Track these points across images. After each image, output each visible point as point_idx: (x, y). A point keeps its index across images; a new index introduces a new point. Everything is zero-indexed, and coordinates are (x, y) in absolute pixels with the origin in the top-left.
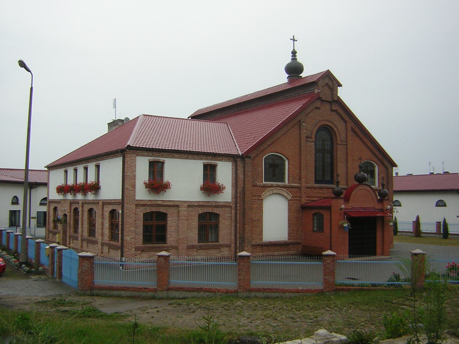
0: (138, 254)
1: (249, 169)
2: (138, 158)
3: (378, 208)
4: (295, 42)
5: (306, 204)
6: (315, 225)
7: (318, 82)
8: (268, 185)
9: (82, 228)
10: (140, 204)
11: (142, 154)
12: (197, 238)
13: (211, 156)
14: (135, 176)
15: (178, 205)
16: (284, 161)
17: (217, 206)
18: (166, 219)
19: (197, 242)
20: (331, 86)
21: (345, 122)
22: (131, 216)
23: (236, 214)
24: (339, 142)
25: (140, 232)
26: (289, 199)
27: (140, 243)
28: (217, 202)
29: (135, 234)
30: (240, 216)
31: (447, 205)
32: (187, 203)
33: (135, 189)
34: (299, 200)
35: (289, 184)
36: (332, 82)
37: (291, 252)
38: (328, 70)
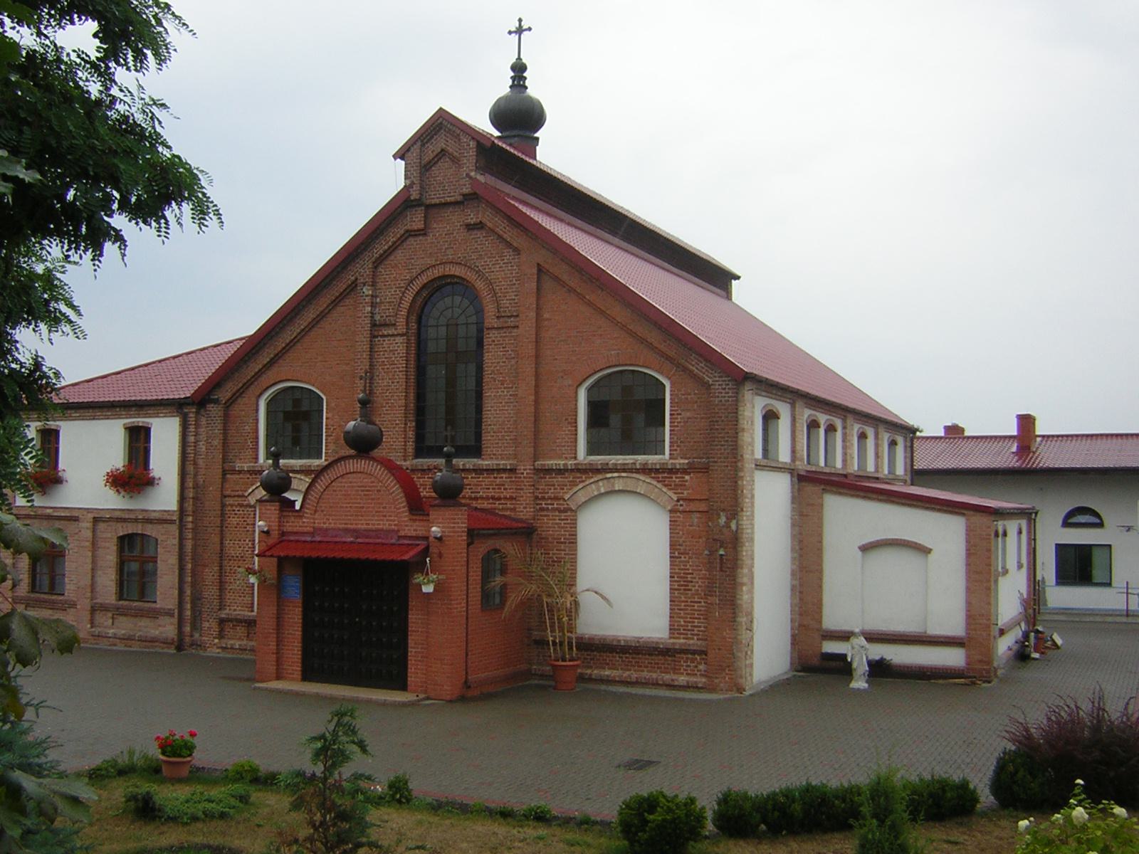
8: (422, 465)
13: (134, 409)
17: (149, 521)
23: (182, 539)
28: (146, 511)
38: (441, 109)
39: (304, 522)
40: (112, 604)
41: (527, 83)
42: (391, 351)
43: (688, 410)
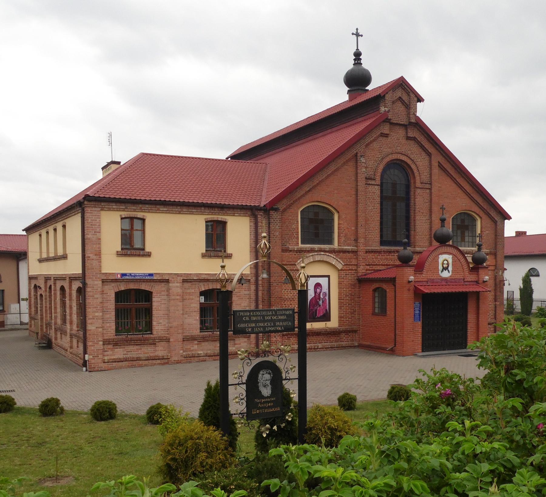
0: (109, 349)
1: (277, 227)
2: (103, 213)
3: (470, 280)
4: (360, 38)
5: (365, 275)
6: (377, 305)
7: (384, 96)
9: (56, 313)
10: (107, 280)
11: (110, 207)
12: (199, 326)
14: (100, 239)
15: (168, 280)
16: (333, 214)
18: (152, 300)
19: (199, 331)
20: (406, 101)
21: (428, 155)
22: (96, 296)
23: (257, 290)
24: (418, 184)
25: (111, 318)
26: (340, 269)
27: (112, 333)
29: (103, 321)
30: (262, 294)
31: (540, 275)
32: (182, 276)
33: (100, 257)
34: (356, 270)
35: (340, 247)
36: (409, 95)
37: (342, 343)
39: (423, 276)
40: (198, 335)
41: (362, 62)
42: (373, 192)
43: (488, 230)
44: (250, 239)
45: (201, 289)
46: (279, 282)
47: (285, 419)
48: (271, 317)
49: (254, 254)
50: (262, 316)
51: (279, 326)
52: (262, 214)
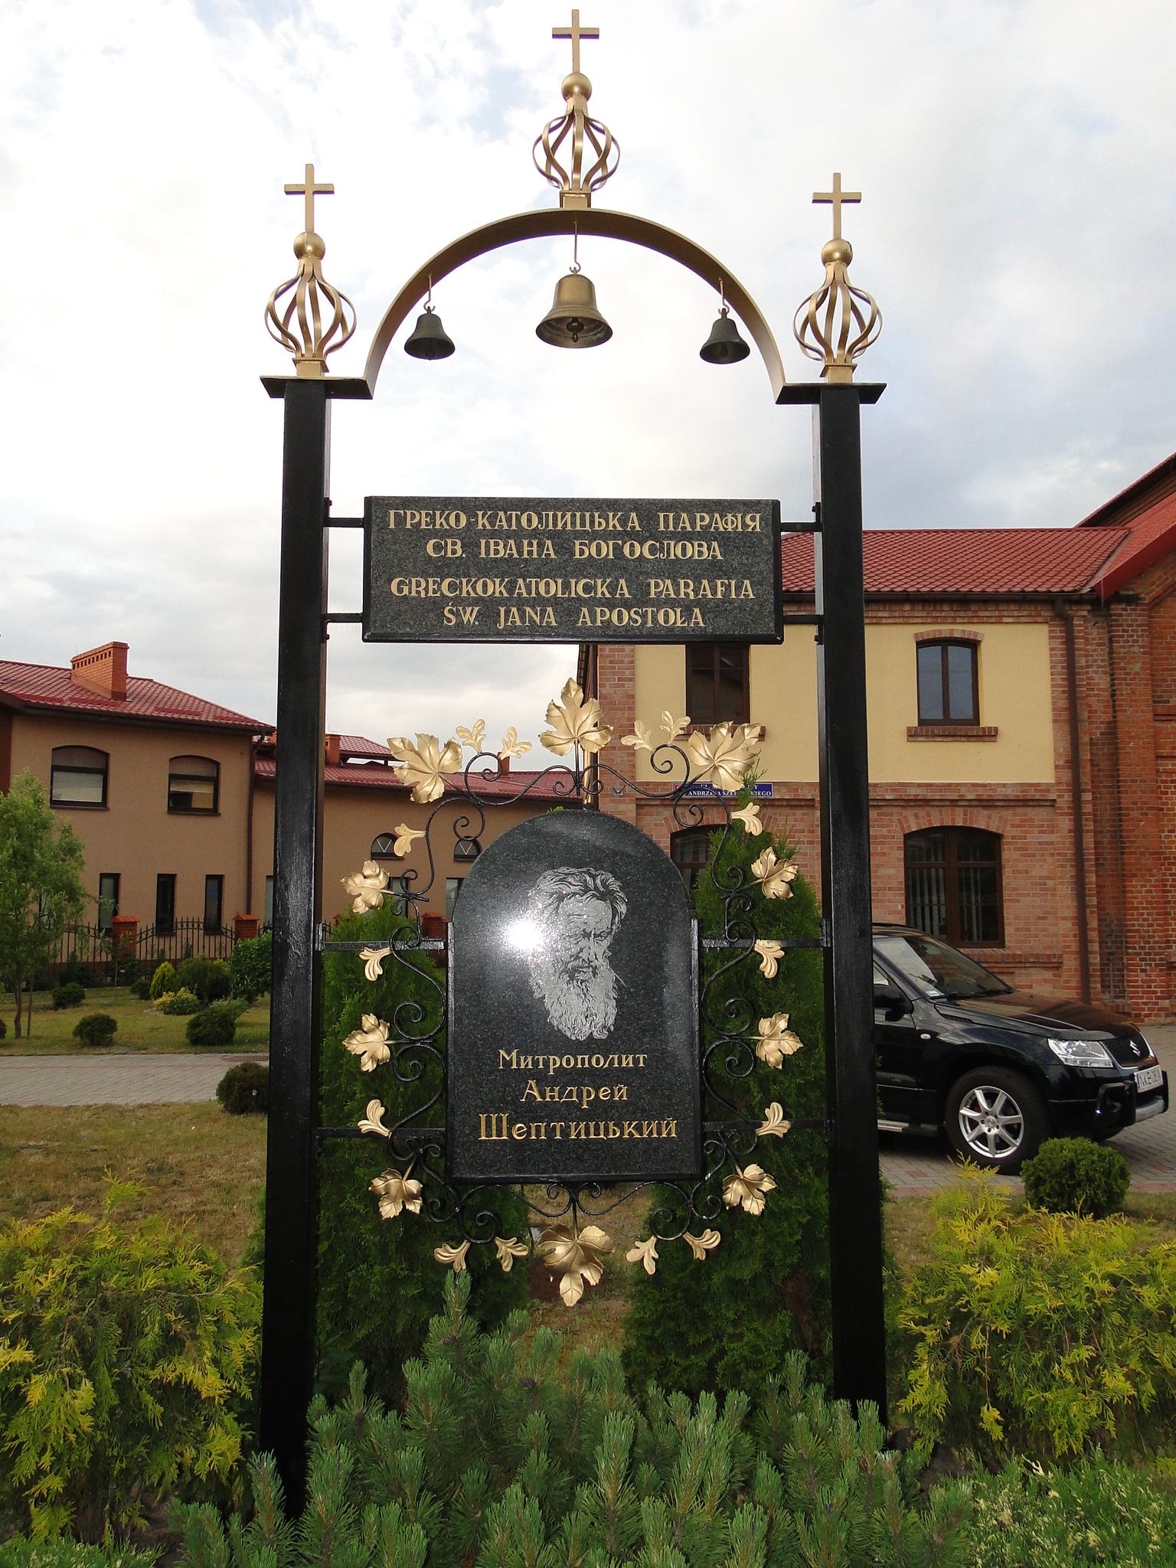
1: (1136, 649)
14: (633, 697)
23: (1078, 832)
44: (1053, 686)
45: (909, 827)
46: (1150, 809)
47: (719, 1203)
48: (618, 549)
49: (1066, 727)
50: (553, 535)
51: (672, 603)
52: (1085, 613)
